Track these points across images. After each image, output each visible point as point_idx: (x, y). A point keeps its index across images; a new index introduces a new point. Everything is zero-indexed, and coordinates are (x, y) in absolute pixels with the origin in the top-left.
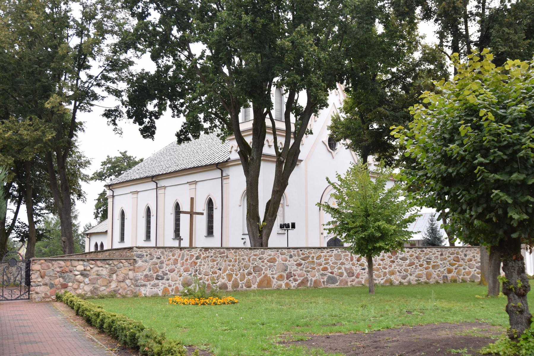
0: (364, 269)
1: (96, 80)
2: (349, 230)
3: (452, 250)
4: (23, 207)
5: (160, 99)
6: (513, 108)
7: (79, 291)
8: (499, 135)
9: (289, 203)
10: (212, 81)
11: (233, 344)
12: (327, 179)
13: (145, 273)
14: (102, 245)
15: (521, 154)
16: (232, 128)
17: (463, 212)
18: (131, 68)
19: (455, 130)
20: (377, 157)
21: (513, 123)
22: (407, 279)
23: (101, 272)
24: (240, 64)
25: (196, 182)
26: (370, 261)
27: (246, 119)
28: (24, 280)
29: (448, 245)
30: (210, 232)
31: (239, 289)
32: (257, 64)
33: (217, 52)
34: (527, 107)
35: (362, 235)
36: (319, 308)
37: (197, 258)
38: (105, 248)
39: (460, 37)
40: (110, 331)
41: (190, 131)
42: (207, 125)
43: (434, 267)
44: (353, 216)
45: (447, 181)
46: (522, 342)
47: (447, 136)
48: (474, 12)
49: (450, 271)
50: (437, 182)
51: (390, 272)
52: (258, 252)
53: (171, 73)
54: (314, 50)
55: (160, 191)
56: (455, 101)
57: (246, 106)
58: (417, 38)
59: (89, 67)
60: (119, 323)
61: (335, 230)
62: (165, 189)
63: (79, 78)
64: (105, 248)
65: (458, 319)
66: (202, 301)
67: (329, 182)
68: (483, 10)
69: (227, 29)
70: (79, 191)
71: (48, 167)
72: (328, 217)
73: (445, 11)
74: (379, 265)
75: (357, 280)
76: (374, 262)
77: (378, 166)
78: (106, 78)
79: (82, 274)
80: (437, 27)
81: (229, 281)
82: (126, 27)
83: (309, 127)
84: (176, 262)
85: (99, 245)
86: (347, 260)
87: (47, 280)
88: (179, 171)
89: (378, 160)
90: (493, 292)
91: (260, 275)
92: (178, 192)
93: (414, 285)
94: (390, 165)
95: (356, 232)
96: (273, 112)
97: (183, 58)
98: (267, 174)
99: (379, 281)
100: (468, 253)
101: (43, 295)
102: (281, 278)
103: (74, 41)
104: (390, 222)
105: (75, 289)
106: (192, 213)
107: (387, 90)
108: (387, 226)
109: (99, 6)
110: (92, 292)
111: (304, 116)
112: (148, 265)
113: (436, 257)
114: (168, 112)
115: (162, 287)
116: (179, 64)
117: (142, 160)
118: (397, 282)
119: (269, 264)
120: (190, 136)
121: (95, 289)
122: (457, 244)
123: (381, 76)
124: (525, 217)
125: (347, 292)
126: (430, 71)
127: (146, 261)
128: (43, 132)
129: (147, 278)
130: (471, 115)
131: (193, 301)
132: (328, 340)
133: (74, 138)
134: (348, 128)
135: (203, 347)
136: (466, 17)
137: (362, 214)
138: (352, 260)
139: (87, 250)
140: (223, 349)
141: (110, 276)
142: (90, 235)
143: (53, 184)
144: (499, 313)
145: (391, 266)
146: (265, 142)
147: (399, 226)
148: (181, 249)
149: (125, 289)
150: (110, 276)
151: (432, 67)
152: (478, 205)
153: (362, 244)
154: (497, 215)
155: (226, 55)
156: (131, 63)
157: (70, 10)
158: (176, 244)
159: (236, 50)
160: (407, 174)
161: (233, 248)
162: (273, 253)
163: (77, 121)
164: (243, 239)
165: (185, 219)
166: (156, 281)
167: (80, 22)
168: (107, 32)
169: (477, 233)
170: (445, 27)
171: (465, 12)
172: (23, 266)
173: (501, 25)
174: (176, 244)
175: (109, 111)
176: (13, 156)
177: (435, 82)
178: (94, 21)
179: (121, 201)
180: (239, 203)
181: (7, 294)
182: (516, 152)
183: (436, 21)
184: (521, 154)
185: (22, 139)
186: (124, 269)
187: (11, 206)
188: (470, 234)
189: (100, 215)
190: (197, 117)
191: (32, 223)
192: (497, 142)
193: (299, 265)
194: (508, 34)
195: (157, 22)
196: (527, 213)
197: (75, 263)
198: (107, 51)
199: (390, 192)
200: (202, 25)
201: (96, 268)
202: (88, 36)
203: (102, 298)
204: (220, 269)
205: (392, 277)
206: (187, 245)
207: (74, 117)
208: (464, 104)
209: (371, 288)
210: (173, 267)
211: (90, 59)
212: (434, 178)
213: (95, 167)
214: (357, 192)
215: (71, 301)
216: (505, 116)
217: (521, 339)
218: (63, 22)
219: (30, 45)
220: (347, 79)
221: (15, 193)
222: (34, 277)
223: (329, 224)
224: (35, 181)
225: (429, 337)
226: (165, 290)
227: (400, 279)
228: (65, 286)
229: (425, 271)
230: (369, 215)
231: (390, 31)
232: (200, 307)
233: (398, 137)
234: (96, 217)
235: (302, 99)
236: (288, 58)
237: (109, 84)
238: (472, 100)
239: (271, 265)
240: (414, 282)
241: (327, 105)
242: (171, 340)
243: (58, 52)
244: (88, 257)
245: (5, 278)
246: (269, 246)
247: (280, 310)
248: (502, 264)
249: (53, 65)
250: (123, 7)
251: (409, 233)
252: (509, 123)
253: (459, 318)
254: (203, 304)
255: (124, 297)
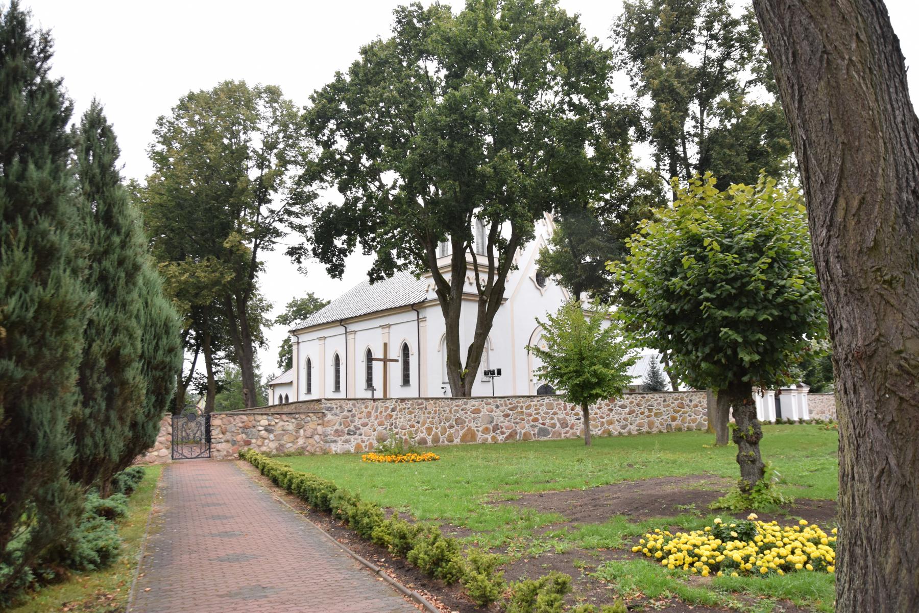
0: (579, 419)
1: (277, 214)
2: (561, 376)
3: (676, 395)
4: (201, 356)
5: (348, 234)
6: (740, 236)
7: (264, 449)
8: (725, 266)
9: (493, 347)
10: (405, 212)
11: (436, 505)
12: (537, 319)
13: (335, 428)
14: (287, 397)
15: (750, 287)
16: (429, 265)
17: (688, 353)
18: (315, 201)
19: (677, 262)
20: (590, 293)
21: (740, 253)
22: (627, 429)
23: (286, 428)
24: (437, 194)
25: (389, 326)
26: (586, 410)
27: (444, 254)
28: (203, 437)
29: (671, 390)
30: (406, 381)
31: (440, 444)
32: (455, 192)
33: (411, 181)
34: (755, 235)
35: (577, 381)
36: (530, 464)
37: (393, 410)
38: (290, 401)
39: (678, 160)
40: (299, 493)
41: (383, 269)
42: (400, 262)
43: (656, 415)
44: (566, 360)
45: (670, 319)
46: (754, 495)
47: (668, 269)
48: (692, 133)
49: (674, 419)
50: (659, 319)
51: (607, 421)
52: (460, 402)
53: (360, 205)
54: (519, 176)
55: (350, 337)
56: (676, 230)
57: (444, 240)
58: (631, 161)
59: (270, 201)
60: (308, 483)
61: (546, 376)
63: (259, 214)
64: (290, 401)
65: (684, 471)
66: (400, 458)
67: (539, 322)
68: (702, 130)
69: (422, 155)
70: (262, 338)
71: (227, 312)
72: (538, 362)
73: (660, 132)
74: (596, 414)
75: (571, 431)
76: (590, 411)
77: (592, 303)
78: (290, 213)
79: (266, 430)
80: (653, 149)
81: (429, 435)
82: (310, 156)
83: (514, 262)
84: (369, 415)
85: (284, 397)
86: (560, 409)
87: (228, 436)
88: (370, 314)
89: (592, 297)
90: (722, 441)
91: (463, 428)
92: (371, 337)
93: (635, 436)
94: (606, 302)
95: (569, 378)
96: (474, 246)
97: (373, 188)
98: (469, 314)
99: (596, 431)
100: (693, 398)
101: (225, 453)
102: (486, 431)
103: (254, 174)
104: (607, 366)
105: (259, 446)
106: (385, 361)
107: (600, 219)
108: (604, 370)
109: (281, 135)
110: (277, 449)
111: (508, 250)
112: (338, 419)
113: (659, 404)
114: (359, 248)
115: (354, 443)
116: (370, 196)
117: (329, 302)
118: (616, 433)
119: (473, 415)
120: (383, 274)
121: (281, 445)
122: (681, 388)
123: (594, 203)
124: (757, 357)
125: (560, 445)
126: (646, 197)
127: (336, 415)
128: (222, 274)
129: (338, 433)
130: (695, 246)
131: (388, 458)
132: (541, 499)
133: (255, 280)
134: (558, 262)
135: (403, 509)
136: (684, 138)
137: (576, 357)
138: (565, 409)
139: (270, 404)
140: (424, 511)
141: (297, 432)
142: (273, 386)
143: (233, 331)
144: (729, 464)
145: (608, 415)
146: (466, 279)
147: (618, 370)
148: (374, 400)
149: (313, 446)
150: (297, 432)
151: (649, 193)
152: (704, 345)
153: (576, 391)
154: (726, 356)
155: (420, 184)
156: (316, 196)
157: (250, 140)
158: (368, 395)
159: (431, 179)
160: (625, 312)
161: (432, 399)
162: (477, 404)
163: (258, 260)
165: (377, 367)
166: (348, 437)
167: (261, 152)
168: (290, 162)
169: (704, 375)
170: (661, 150)
171: (683, 132)
172: (203, 420)
173: (722, 147)
174: (368, 395)
175: (293, 248)
176: (190, 301)
177: (654, 210)
178: (275, 151)
179: (309, 348)
180: (437, 348)
181: (186, 452)
182: (744, 285)
183: (651, 142)
184: (750, 287)
185: (200, 282)
186: (312, 423)
187: (188, 355)
188: (697, 376)
189: (284, 364)
190: (390, 253)
191: (211, 374)
192: (723, 274)
193: (507, 416)
194: (730, 156)
195: (344, 150)
196: (758, 353)
197: (259, 418)
198: (289, 183)
199: (606, 332)
200: (393, 152)
201: (281, 423)
202: (269, 167)
203: (289, 455)
204: (418, 422)
205: (611, 427)
206: (381, 396)
207: (254, 257)
208: (687, 233)
209: (588, 440)
210: (366, 420)
211: (271, 192)
212: (656, 316)
213: (280, 309)
214: (570, 333)
215: (256, 460)
216: (731, 246)
217: (753, 491)
218: (241, 153)
219: (207, 179)
220: (556, 208)
221: (192, 341)
222: (215, 433)
223: (539, 369)
224: (214, 328)
225: (653, 492)
226: (358, 447)
227: (619, 429)
228: (248, 443)
229: (646, 420)
230: (583, 359)
231: (602, 154)
232: (397, 465)
233: (614, 270)
234: (280, 366)
235: (506, 230)
236: (490, 186)
237: (293, 219)
238: (695, 228)
239: (475, 417)
240: (634, 432)
241: (534, 238)
242: (367, 502)
243: (236, 186)
244: (272, 411)
245: (184, 434)
246: (473, 395)
247: (486, 467)
248: (731, 410)
249: (231, 200)
250: (307, 135)
251: (628, 378)
252: (736, 253)
253: (686, 470)
254: (401, 461)
255: (313, 454)
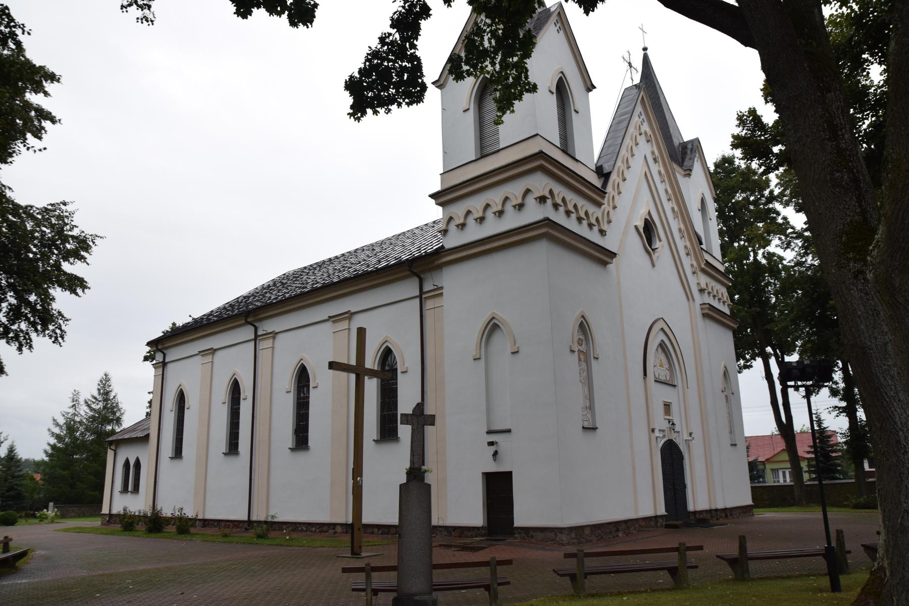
55: (264, 344)
62: (274, 338)
85: (132, 463)
164: (491, 444)
